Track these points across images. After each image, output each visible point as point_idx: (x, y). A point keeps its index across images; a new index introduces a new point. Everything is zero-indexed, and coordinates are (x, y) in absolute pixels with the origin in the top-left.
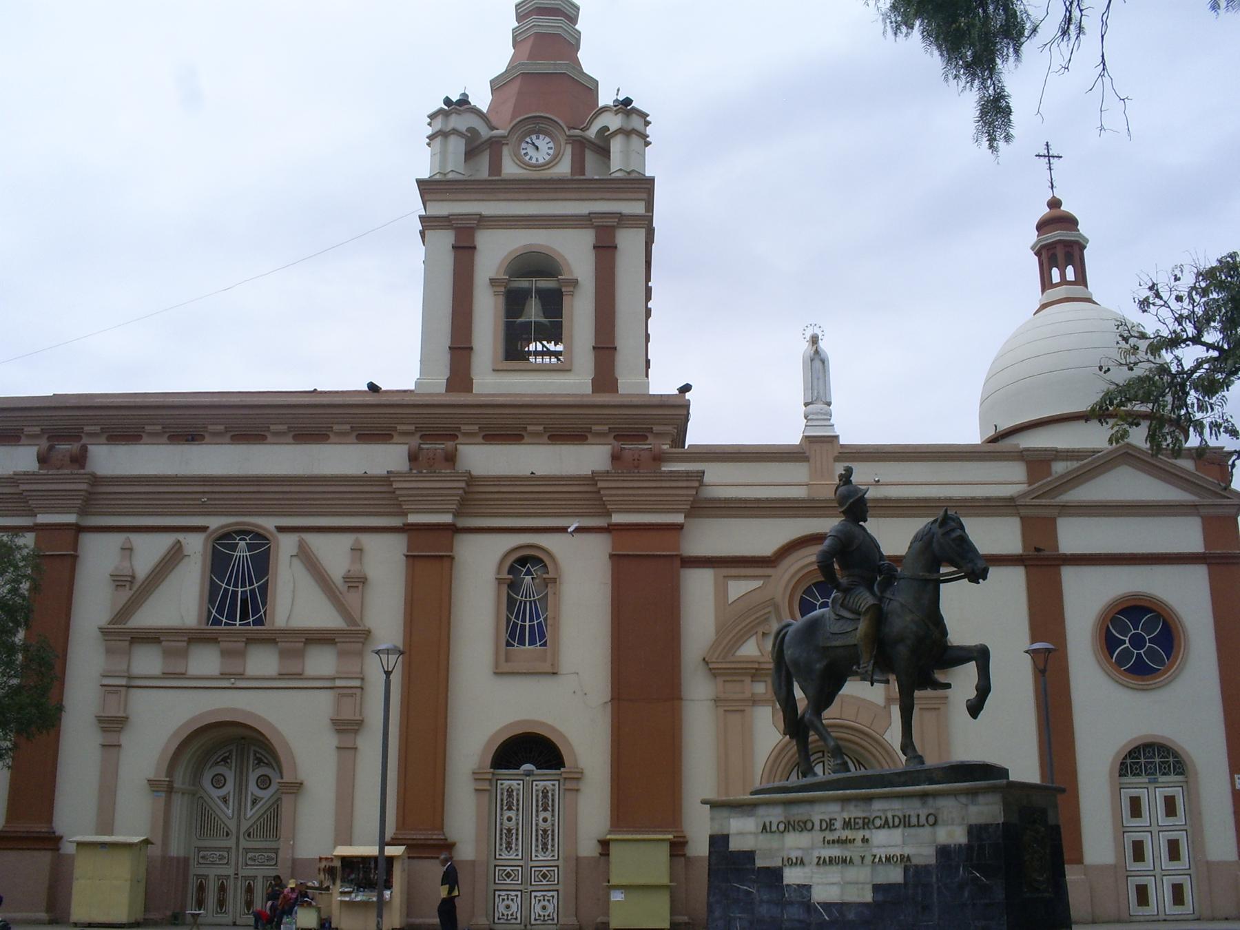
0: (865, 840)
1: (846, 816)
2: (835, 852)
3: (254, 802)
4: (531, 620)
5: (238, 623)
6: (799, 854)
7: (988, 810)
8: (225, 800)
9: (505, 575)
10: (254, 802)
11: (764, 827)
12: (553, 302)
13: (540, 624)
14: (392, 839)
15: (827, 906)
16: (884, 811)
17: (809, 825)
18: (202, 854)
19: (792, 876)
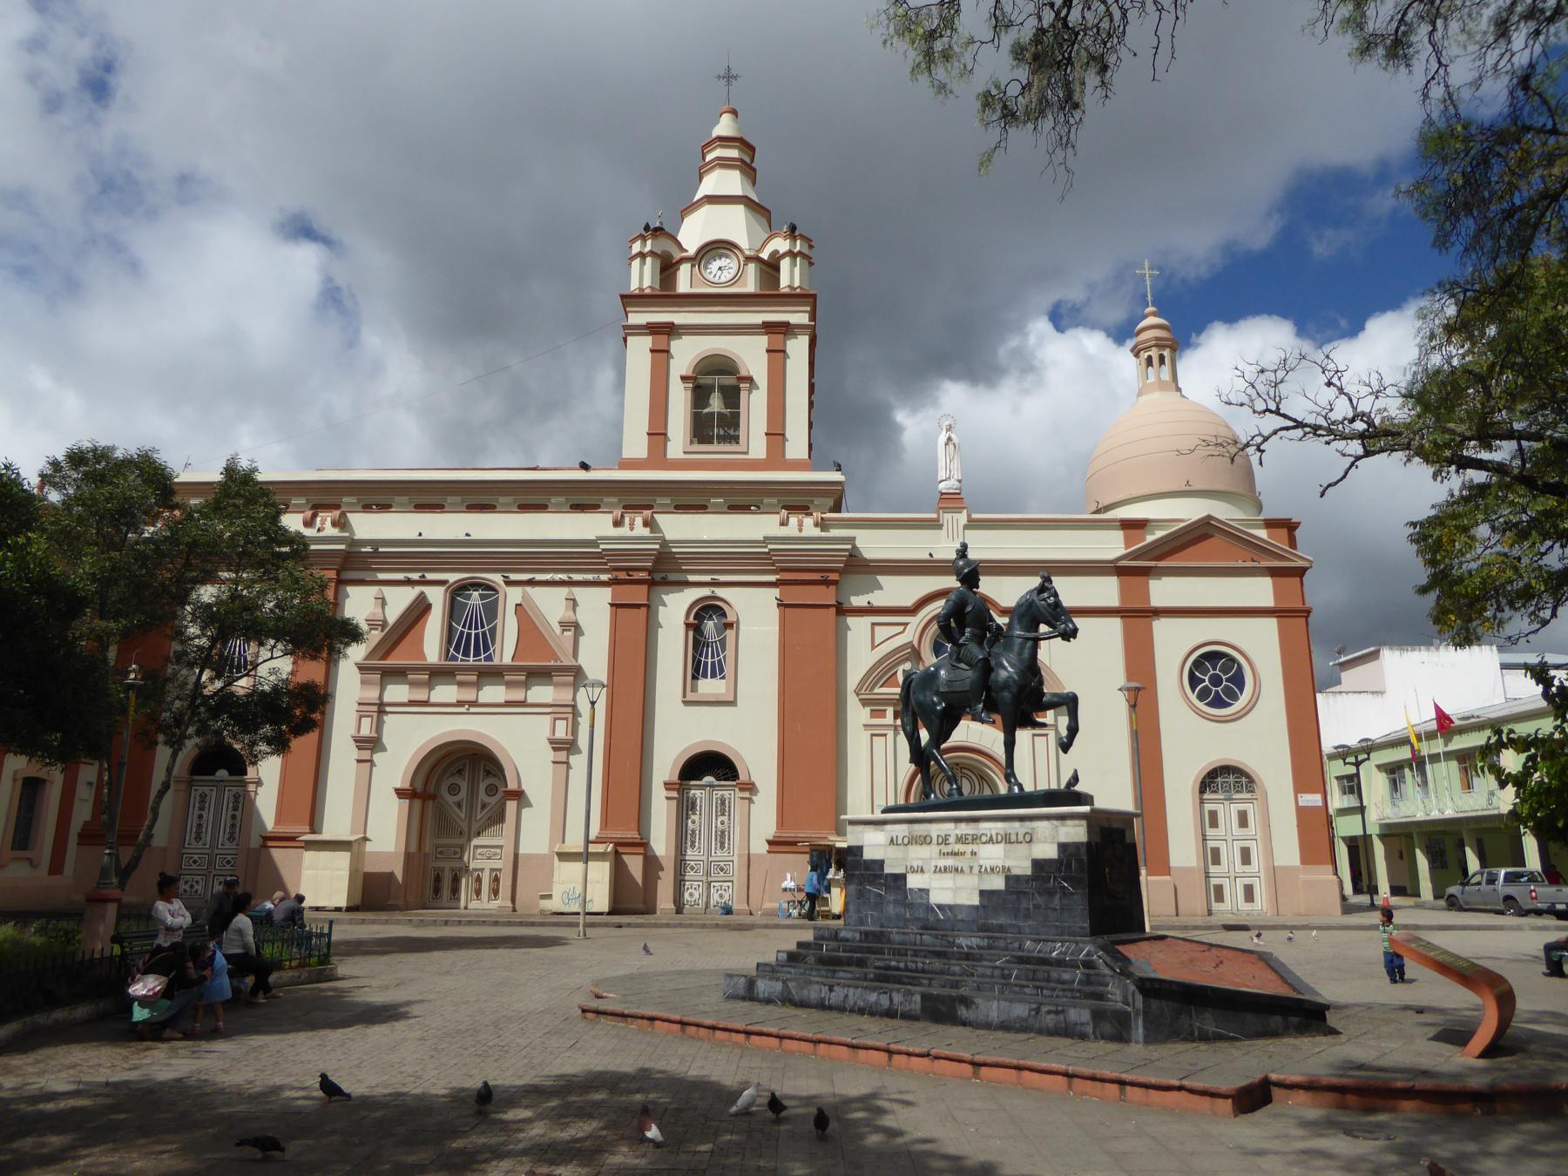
0: (974, 854)
1: (959, 832)
2: (950, 862)
3: (484, 806)
4: (713, 657)
5: (472, 659)
6: (920, 863)
7: (1076, 833)
8: (459, 805)
9: (691, 619)
10: (484, 806)
11: (892, 840)
12: (732, 396)
13: (720, 661)
14: (597, 838)
15: (940, 907)
16: (990, 829)
17: (928, 840)
18: (439, 850)
19: (914, 882)
